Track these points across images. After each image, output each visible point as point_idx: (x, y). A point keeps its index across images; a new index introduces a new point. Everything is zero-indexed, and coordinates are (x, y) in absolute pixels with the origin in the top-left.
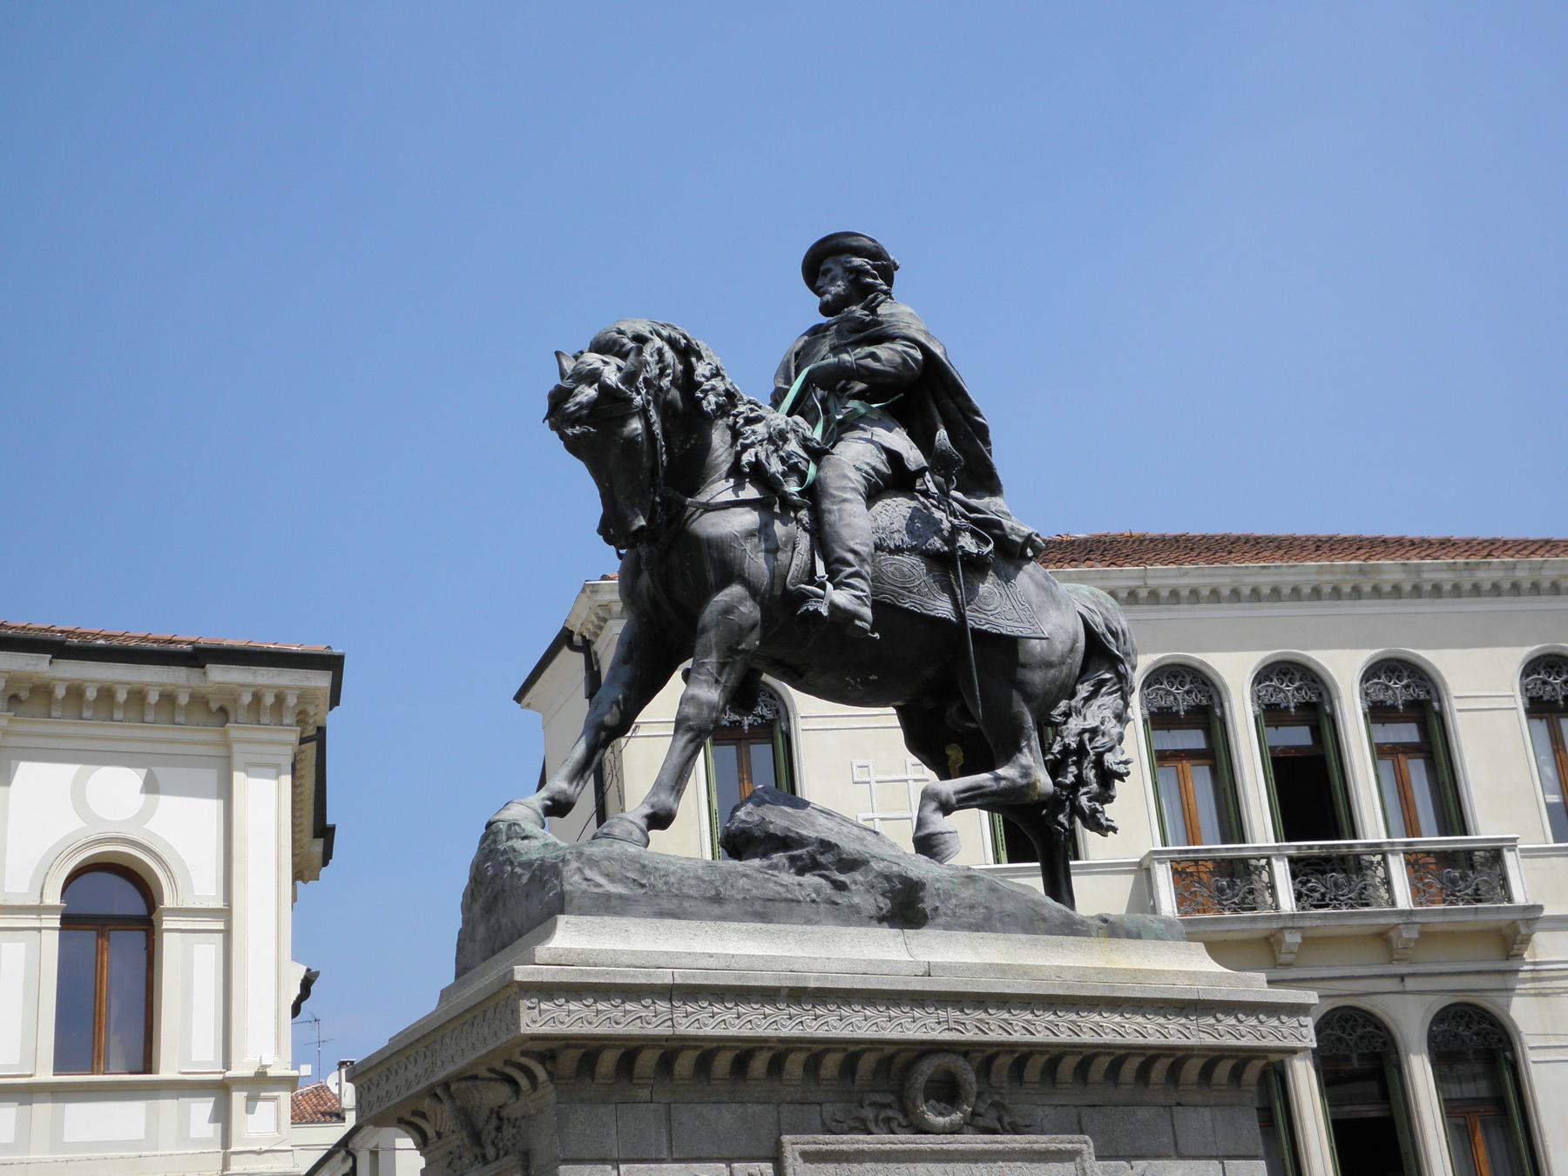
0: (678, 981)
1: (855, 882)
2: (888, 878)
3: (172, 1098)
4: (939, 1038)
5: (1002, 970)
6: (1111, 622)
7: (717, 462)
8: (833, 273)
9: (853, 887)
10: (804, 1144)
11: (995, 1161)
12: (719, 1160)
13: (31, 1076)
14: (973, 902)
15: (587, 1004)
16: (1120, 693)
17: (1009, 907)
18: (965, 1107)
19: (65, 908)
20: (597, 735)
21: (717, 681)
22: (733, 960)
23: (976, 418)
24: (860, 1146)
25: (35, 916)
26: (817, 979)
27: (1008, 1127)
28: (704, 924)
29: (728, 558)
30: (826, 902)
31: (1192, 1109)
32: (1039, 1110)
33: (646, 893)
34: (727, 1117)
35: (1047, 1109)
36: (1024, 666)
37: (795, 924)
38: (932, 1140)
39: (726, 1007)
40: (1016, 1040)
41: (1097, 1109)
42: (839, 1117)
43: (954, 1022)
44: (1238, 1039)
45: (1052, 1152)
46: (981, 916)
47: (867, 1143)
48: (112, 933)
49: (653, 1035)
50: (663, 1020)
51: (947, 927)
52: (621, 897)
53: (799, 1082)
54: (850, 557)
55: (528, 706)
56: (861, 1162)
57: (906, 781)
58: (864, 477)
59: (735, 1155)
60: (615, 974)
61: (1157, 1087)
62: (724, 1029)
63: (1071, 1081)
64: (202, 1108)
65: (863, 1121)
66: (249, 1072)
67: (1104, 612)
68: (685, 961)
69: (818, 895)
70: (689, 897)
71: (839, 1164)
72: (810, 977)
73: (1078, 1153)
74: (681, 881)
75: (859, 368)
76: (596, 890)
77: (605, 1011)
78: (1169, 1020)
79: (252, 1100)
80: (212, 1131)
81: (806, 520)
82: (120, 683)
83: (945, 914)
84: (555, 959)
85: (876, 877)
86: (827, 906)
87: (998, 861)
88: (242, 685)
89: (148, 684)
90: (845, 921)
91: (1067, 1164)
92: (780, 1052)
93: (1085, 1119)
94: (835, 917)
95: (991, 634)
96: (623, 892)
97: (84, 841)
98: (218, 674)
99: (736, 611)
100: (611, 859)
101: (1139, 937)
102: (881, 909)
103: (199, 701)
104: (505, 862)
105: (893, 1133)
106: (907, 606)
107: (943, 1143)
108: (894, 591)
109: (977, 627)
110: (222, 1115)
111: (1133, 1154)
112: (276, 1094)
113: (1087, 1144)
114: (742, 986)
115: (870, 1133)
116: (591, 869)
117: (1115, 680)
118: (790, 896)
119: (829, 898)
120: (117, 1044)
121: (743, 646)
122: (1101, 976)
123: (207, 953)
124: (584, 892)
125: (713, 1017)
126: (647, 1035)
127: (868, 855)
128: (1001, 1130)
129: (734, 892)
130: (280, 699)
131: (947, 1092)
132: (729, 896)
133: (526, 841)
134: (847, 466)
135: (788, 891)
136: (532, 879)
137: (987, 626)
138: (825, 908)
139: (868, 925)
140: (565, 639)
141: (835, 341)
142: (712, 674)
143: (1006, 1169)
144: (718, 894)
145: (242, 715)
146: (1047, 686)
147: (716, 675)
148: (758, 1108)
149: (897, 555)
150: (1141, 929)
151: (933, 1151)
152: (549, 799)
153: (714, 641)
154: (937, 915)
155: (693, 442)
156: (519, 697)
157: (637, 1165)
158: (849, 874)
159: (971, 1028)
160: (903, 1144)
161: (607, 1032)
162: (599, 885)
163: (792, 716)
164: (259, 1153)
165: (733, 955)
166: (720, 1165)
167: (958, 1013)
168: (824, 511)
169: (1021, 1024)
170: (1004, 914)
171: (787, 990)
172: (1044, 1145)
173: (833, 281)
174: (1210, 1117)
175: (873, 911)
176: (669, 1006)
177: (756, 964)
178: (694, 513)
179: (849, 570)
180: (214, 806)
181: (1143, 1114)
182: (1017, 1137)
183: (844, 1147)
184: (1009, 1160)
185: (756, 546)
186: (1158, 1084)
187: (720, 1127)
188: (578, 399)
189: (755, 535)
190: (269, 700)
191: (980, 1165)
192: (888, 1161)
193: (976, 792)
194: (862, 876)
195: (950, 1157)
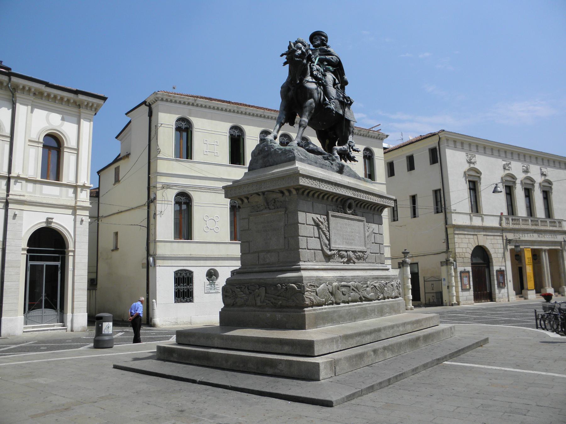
2: (339, 164)
3: (65, 187)
8: (317, 39)
13: (36, 178)
18: (352, 210)
19: (44, 143)
20: (281, 124)
21: (308, 118)
34: (320, 206)
42: (335, 209)
52: (303, 159)
54: (333, 98)
55: (129, 116)
57: (214, 145)
64: (71, 190)
70: (312, 161)
73: (364, 221)
74: (311, 158)
79: (82, 190)
80: (73, 195)
81: (322, 88)
82: (59, 95)
87: (229, 164)
88: (85, 100)
89: (65, 96)
93: (364, 215)
94: (331, 170)
97: (48, 129)
98: (81, 97)
103: (75, 102)
104: (271, 148)
105: (342, 213)
110: (75, 192)
115: (339, 212)
120: (52, 173)
123: (73, 158)
133: (275, 144)
136: (282, 152)
140: (144, 103)
141: (320, 53)
144: (316, 162)
145: (84, 106)
151: (347, 218)
153: (308, 110)
156: (126, 114)
162: (300, 156)
163: (193, 128)
164: (83, 201)
168: (327, 88)
173: (317, 40)
175: (336, 170)
178: (305, 82)
179: (333, 101)
180: (76, 126)
188: (298, 52)
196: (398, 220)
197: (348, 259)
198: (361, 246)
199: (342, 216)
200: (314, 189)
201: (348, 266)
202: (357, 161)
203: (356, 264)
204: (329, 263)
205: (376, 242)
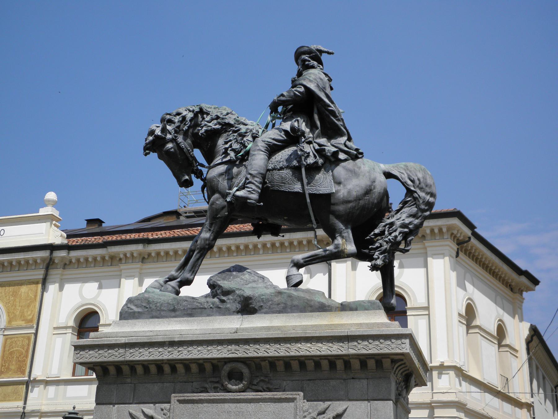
0: (127, 342)
1: (229, 299)
4: (227, 357)
5: (268, 328)
6: (411, 176)
7: (219, 150)
9: (228, 301)
10: (179, 397)
11: (259, 402)
12: (152, 403)
14: (279, 302)
15: (194, 348)
16: (415, 205)
17: (296, 303)
18: (244, 382)
22: (159, 332)
23: (329, 108)
24: (201, 398)
25: (65, 330)
26: (179, 337)
27: (266, 389)
28: (164, 319)
29: (213, 185)
30: (216, 308)
31: (357, 380)
32: (284, 382)
33: (148, 310)
34: (156, 388)
35: (288, 382)
36: (334, 204)
37: (203, 317)
40: (260, 356)
41: (312, 381)
43: (235, 350)
44: (368, 351)
46: (282, 307)
47: (204, 396)
48: (395, 317)
49: (117, 361)
50: (353, 348)
51: (266, 313)
52: (139, 312)
53: (184, 375)
56: (202, 403)
58: (266, 144)
59: (157, 401)
60: (104, 340)
62: (143, 357)
63: (299, 370)
65: (206, 388)
66: (437, 364)
67: (409, 172)
68: (141, 334)
69: (213, 305)
70: (164, 310)
72: (176, 337)
74: (161, 305)
75: (278, 101)
76: (131, 311)
77: (102, 353)
78: (334, 344)
79: (440, 374)
83: (265, 308)
84: (96, 337)
85: (237, 296)
86: (217, 309)
90: (223, 314)
91: (290, 404)
92: (173, 364)
94: (219, 313)
95: (317, 194)
96: (140, 311)
99: (215, 203)
100: (138, 299)
101: (356, 309)
102: (237, 308)
106: (283, 190)
108: (278, 185)
109: (311, 192)
111: (325, 399)
112: (448, 372)
114: (150, 342)
116: (130, 304)
117: (413, 200)
118: (202, 307)
119: (217, 306)
121: (219, 216)
122: (314, 328)
124: (126, 312)
125: (140, 353)
126: (115, 361)
127: (234, 289)
128: (262, 390)
129: (180, 307)
130: (440, 230)
131: (236, 376)
132: (178, 309)
134: (259, 141)
135: (201, 305)
137: (316, 191)
138: (216, 310)
139: (233, 314)
142: (207, 228)
143: (271, 405)
144: (174, 307)
146: (348, 210)
147: (209, 228)
148: (168, 384)
149: (281, 170)
150: (358, 306)
151: (231, 399)
152: (167, 278)
154: (262, 309)
155: (209, 145)
157: (121, 405)
158: (227, 296)
159: (241, 352)
160: (218, 396)
161: (101, 361)
164: (443, 393)
165: (159, 331)
166: (151, 405)
167: (237, 347)
169: (243, 350)
170: (293, 306)
171: (168, 342)
172: (279, 396)
176: (124, 350)
177: (167, 333)
181: (333, 383)
183: (194, 398)
184: (264, 402)
185: (223, 179)
186: (341, 370)
189: (223, 175)
190: (436, 231)
191: (252, 404)
192: (213, 403)
193: (315, 257)
194: (232, 297)
195: (239, 401)
196: (499, 352)
202: (368, 266)
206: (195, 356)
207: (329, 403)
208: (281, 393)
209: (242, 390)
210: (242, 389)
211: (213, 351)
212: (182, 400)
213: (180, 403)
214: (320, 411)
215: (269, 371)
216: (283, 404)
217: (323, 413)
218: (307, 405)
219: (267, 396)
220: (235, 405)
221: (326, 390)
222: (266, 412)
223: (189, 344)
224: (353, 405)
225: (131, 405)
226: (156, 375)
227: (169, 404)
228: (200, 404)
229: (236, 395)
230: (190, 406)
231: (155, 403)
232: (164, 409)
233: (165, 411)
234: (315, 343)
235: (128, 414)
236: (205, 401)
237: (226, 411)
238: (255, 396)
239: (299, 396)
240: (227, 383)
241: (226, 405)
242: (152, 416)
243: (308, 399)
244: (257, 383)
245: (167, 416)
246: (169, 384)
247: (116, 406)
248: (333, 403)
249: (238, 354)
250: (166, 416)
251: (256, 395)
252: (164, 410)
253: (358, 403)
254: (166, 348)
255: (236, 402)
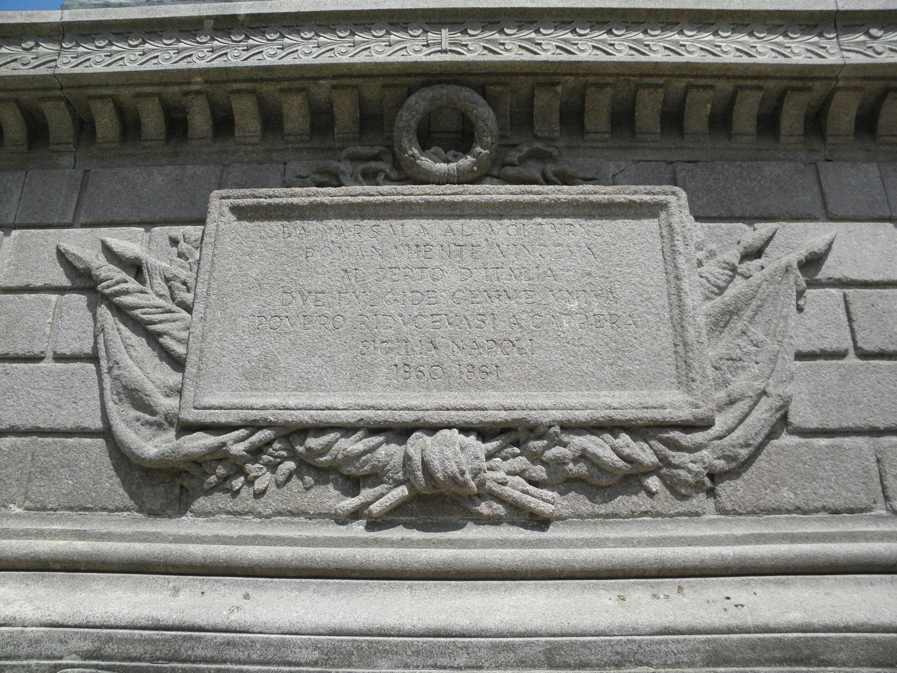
11: (531, 217)
18: (479, 149)
24: (318, 199)
27: (554, 178)
38: (428, 191)
39: (130, 45)
45: (621, 205)
53: (256, 140)
61: (793, 140)
63: (659, 131)
71: (289, 222)
73: (663, 206)
91: (645, 222)
107: (445, 194)
111: (756, 215)
113: (677, 195)
114: (149, 19)
151: (428, 203)
171: (212, 22)
172: (607, 197)
174: (878, 174)
182: (565, 187)
183: (295, 200)
184: (551, 216)
187: (146, 190)
191: (506, 222)
197: (411, 488)
198: (623, 387)
199: (248, 191)
200: (489, 74)
201: (539, 544)
203: (553, 533)
204: (186, 525)
205: (868, 347)
206: (306, 58)
207: (764, 229)
208: (610, 188)
209: (470, 177)
210: (472, 171)
211: (372, 45)
212: (248, 206)
213: (239, 219)
214: (750, 246)
215: (558, 128)
216: (620, 222)
217: (754, 253)
218: (700, 230)
219: (563, 197)
220: (444, 223)
221: (753, 190)
222: (559, 245)
223: (284, 27)
224: (849, 232)
225: (66, 230)
226: (160, 140)
227: (202, 227)
228: (314, 222)
229: (448, 192)
230: (275, 226)
231: (148, 224)
232: (181, 238)
233: (183, 246)
234: (728, 32)
235: (55, 256)
236: (331, 213)
237: (411, 243)
238: (520, 196)
239: (675, 198)
240: (416, 151)
241: (412, 226)
242: (136, 258)
243: (697, 215)
244: (520, 159)
245: (190, 260)
246: (202, 168)
247: (15, 233)
248: (784, 226)
249: (465, 53)
250: (187, 259)
251: (523, 193)
252: (182, 242)
253: (867, 228)
254: (204, 41)
255: (448, 213)
